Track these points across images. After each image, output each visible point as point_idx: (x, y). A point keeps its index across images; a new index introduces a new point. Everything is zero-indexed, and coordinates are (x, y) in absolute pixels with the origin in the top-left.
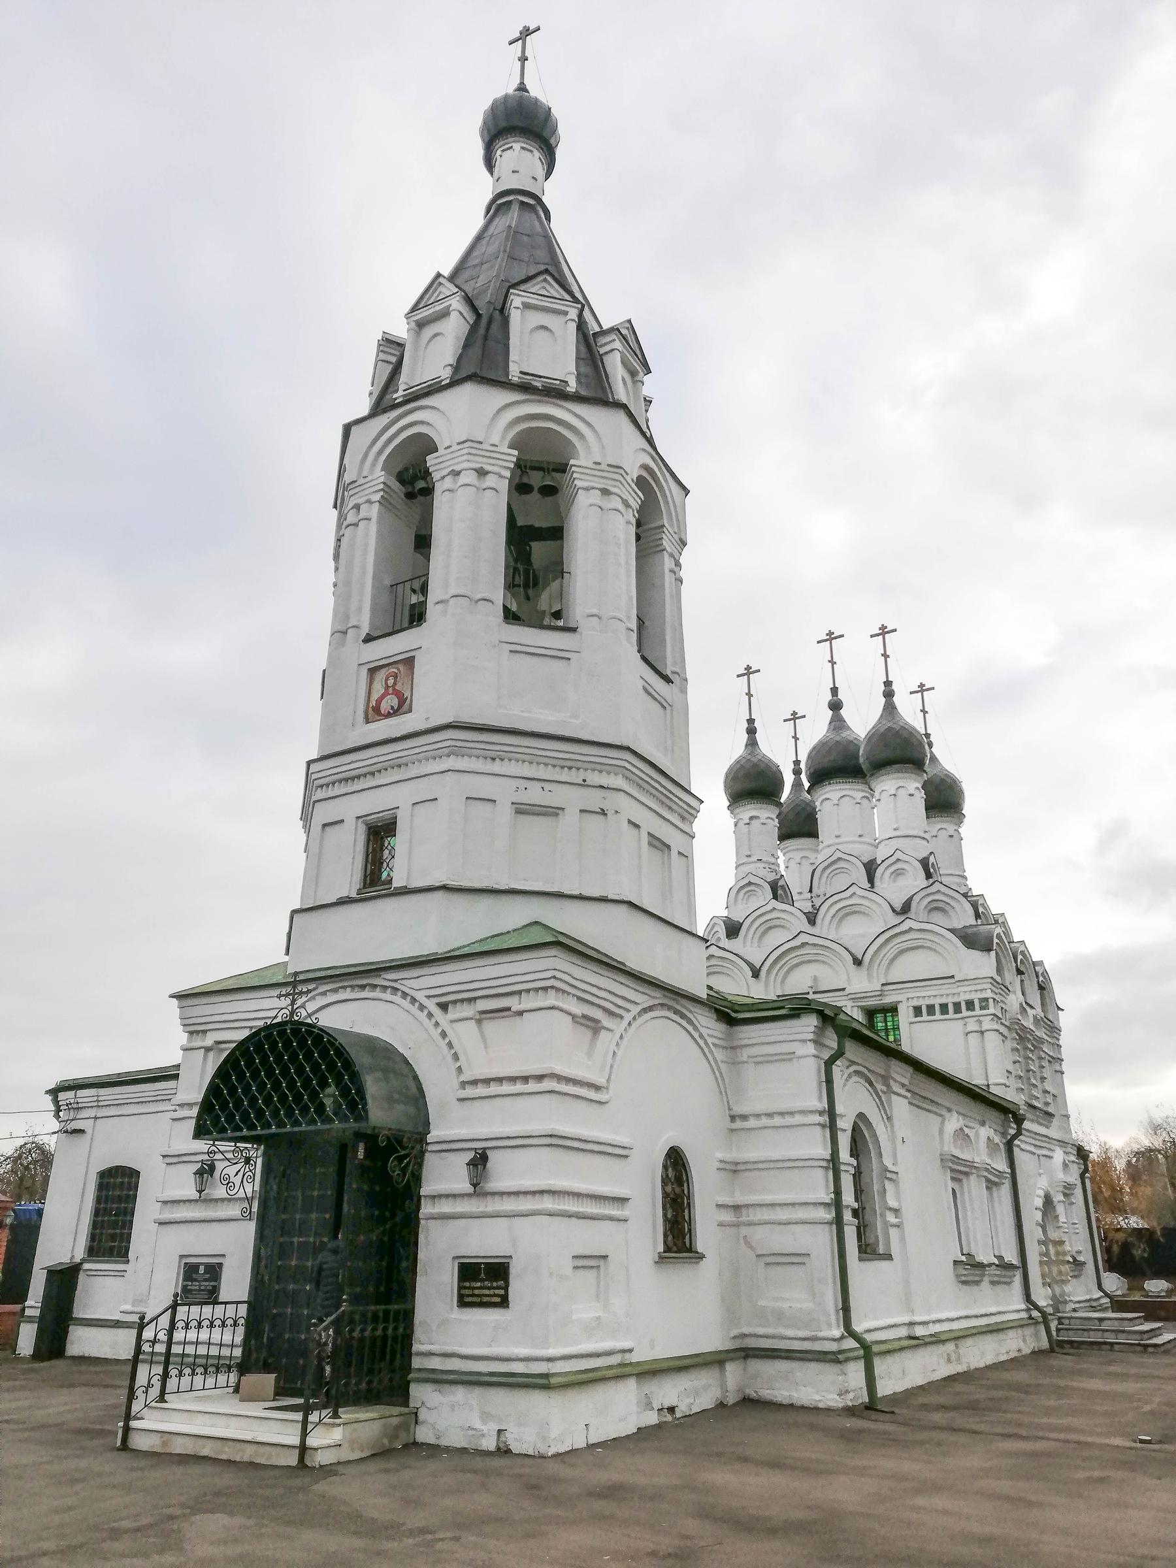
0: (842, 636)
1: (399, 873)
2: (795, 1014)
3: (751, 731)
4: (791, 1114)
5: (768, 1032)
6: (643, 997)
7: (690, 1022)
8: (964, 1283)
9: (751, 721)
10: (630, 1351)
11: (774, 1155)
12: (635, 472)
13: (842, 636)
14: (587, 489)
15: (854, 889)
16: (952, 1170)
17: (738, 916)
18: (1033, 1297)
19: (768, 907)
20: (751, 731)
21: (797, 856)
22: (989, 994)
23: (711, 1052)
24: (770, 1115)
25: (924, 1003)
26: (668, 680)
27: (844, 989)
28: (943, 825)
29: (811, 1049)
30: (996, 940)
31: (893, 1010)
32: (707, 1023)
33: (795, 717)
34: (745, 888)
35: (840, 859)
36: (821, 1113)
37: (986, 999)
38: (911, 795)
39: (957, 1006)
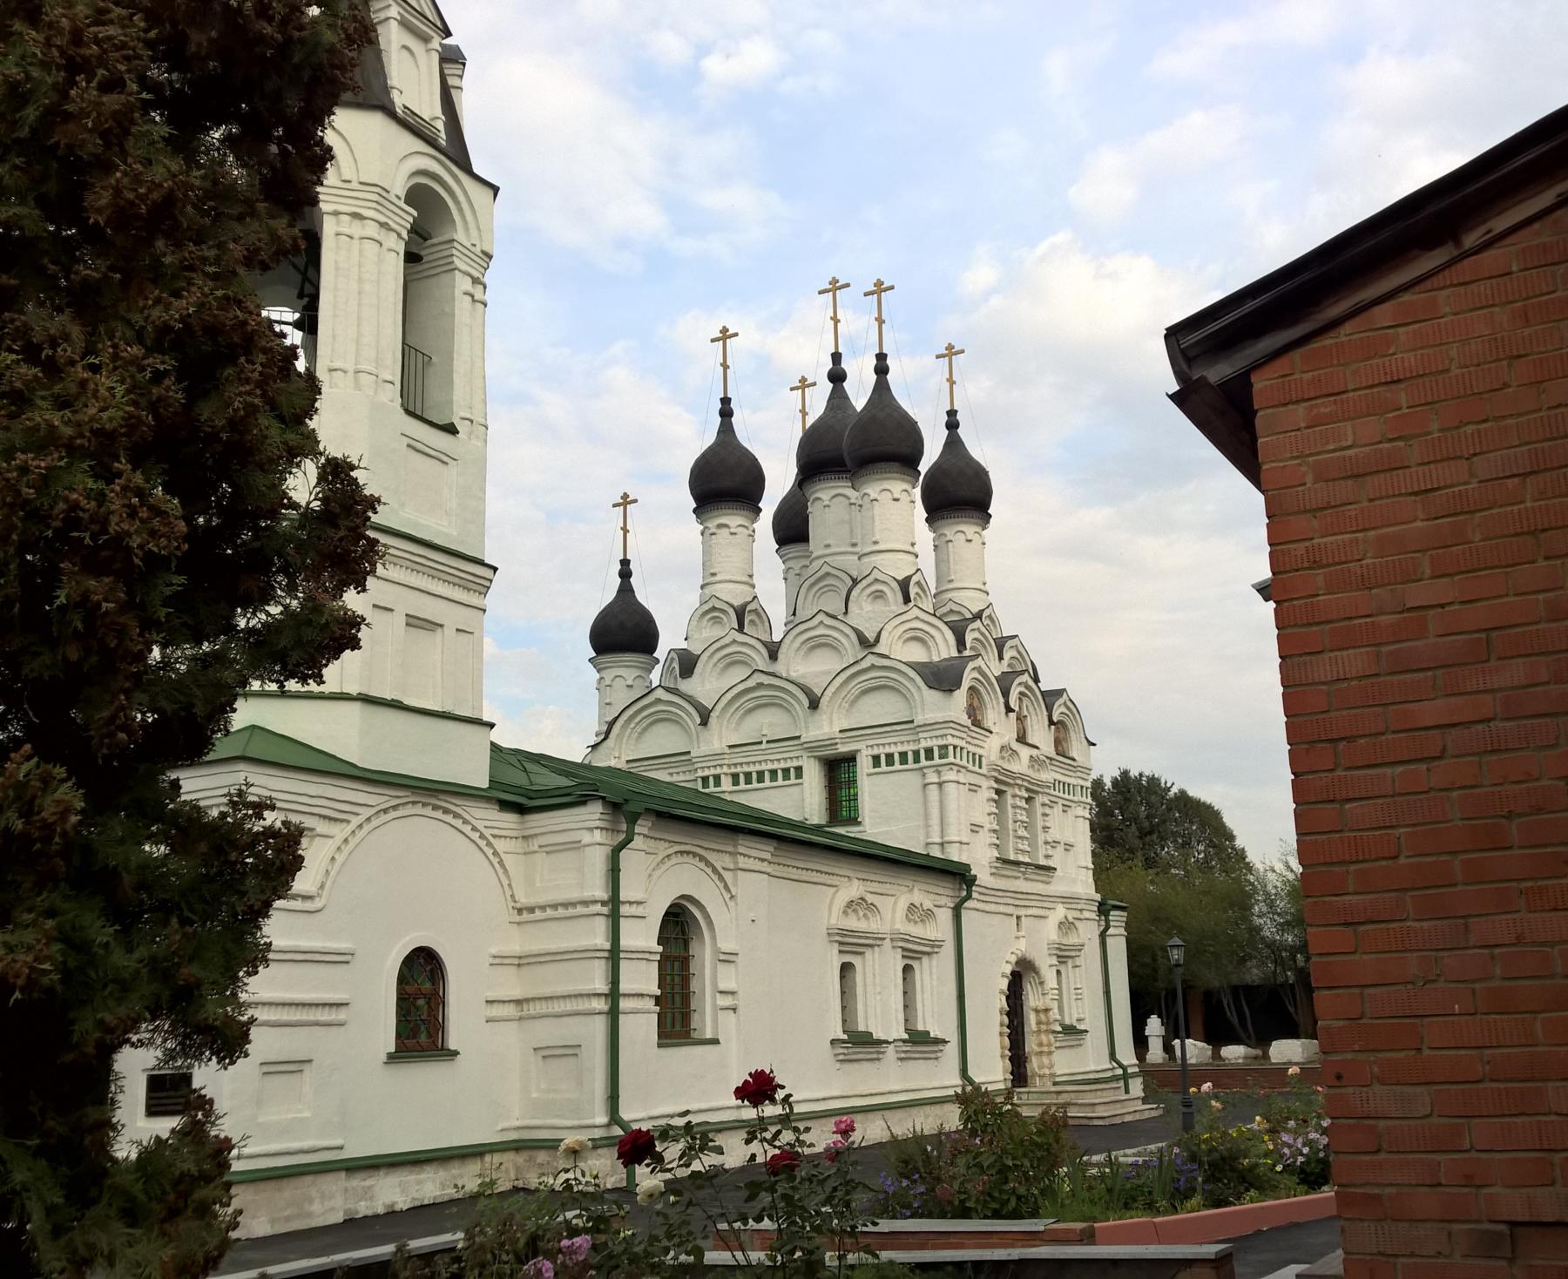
0: (848, 285)
2: (582, 801)
3: (726, 413)
4: (574, 905)
5: (566, 819)
6: (374, 798)
7: (457, 816)
8: (901, 1059)
9: (726, 401)
10: (341, 1148)
11: (553, 947)
12: (399, 188)
13: (848, 285)
14: (336, 213)
15: (821, 617)
16: (841, 943)
17: (696, 649)
18: (970, 1073)
19: (727, 640)
20: (726, 413)
21: (796, 565)
22: (950, 740)
23: (489, 844)
24: (555, 906)
25: (882, 751)
26: (451, 429)
27: (798, 737)
28: (961, 531)
29: (598, 836)
31: (851, 759)
32: (488, 817)
34: (710, 611)
35: (828, 574)
36: (604, 903)
37: (946, 747)
38: (896, 500)
39: (916, 753)
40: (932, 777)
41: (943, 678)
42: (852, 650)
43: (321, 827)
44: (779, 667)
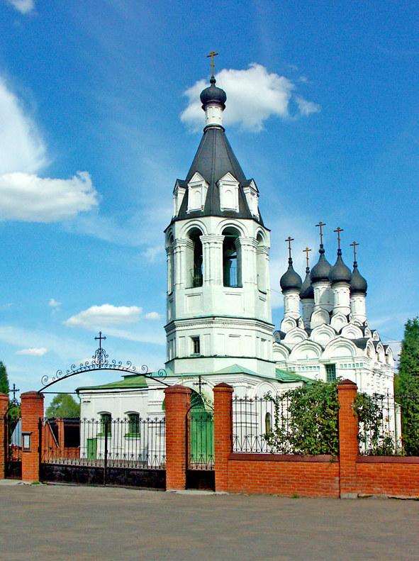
1: (203, 352)
30: (368, 343)
33: (290, 239)
40: (358, 371)
41: (361, 344)
42: (333, 336)
43: (252, 386)
44: (310, 338)
